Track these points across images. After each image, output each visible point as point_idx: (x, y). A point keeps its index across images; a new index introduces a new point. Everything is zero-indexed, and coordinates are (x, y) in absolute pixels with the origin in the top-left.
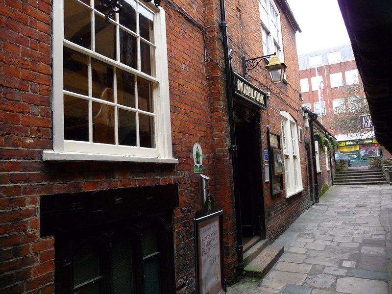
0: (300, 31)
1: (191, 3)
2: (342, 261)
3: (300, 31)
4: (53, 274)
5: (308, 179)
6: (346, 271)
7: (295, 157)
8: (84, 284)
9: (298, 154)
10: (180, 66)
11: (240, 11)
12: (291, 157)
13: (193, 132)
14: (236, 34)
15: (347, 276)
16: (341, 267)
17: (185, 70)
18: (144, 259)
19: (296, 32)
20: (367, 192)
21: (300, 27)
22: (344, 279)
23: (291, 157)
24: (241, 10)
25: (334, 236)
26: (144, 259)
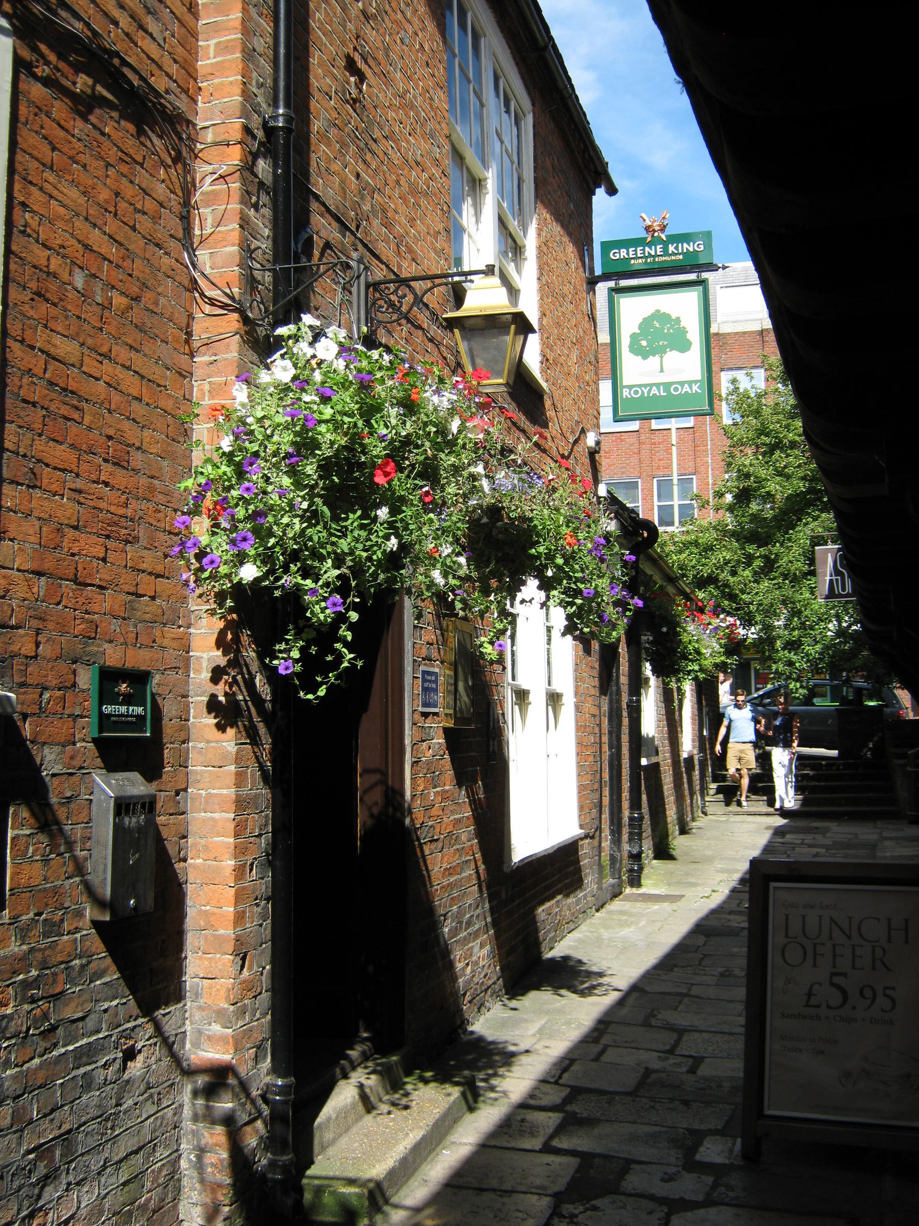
0: (612, 191)
1: (140, 11)
2: (697, 1137)
3: (612, 191)
4: (90, 81)
5: (606, 792)
6: (710, 1180)
7: (554, 699)
8: (839, 783)
9: (565, 684)
10: (65, 277)
11: (362, 77)
12: (538, 700)
13: (103, 574)
14: (337, 166)
15: (709, 1202)
16: (692, 1165)
17: (85, 295)
18: (834, 753)
19: (598, 191)
20: (827, 848)
21: (615, 172)
22: (701, 1212)
23: (538, 700)
24: (368, 72)
25: (681, 1032)
26: (911, 716)
